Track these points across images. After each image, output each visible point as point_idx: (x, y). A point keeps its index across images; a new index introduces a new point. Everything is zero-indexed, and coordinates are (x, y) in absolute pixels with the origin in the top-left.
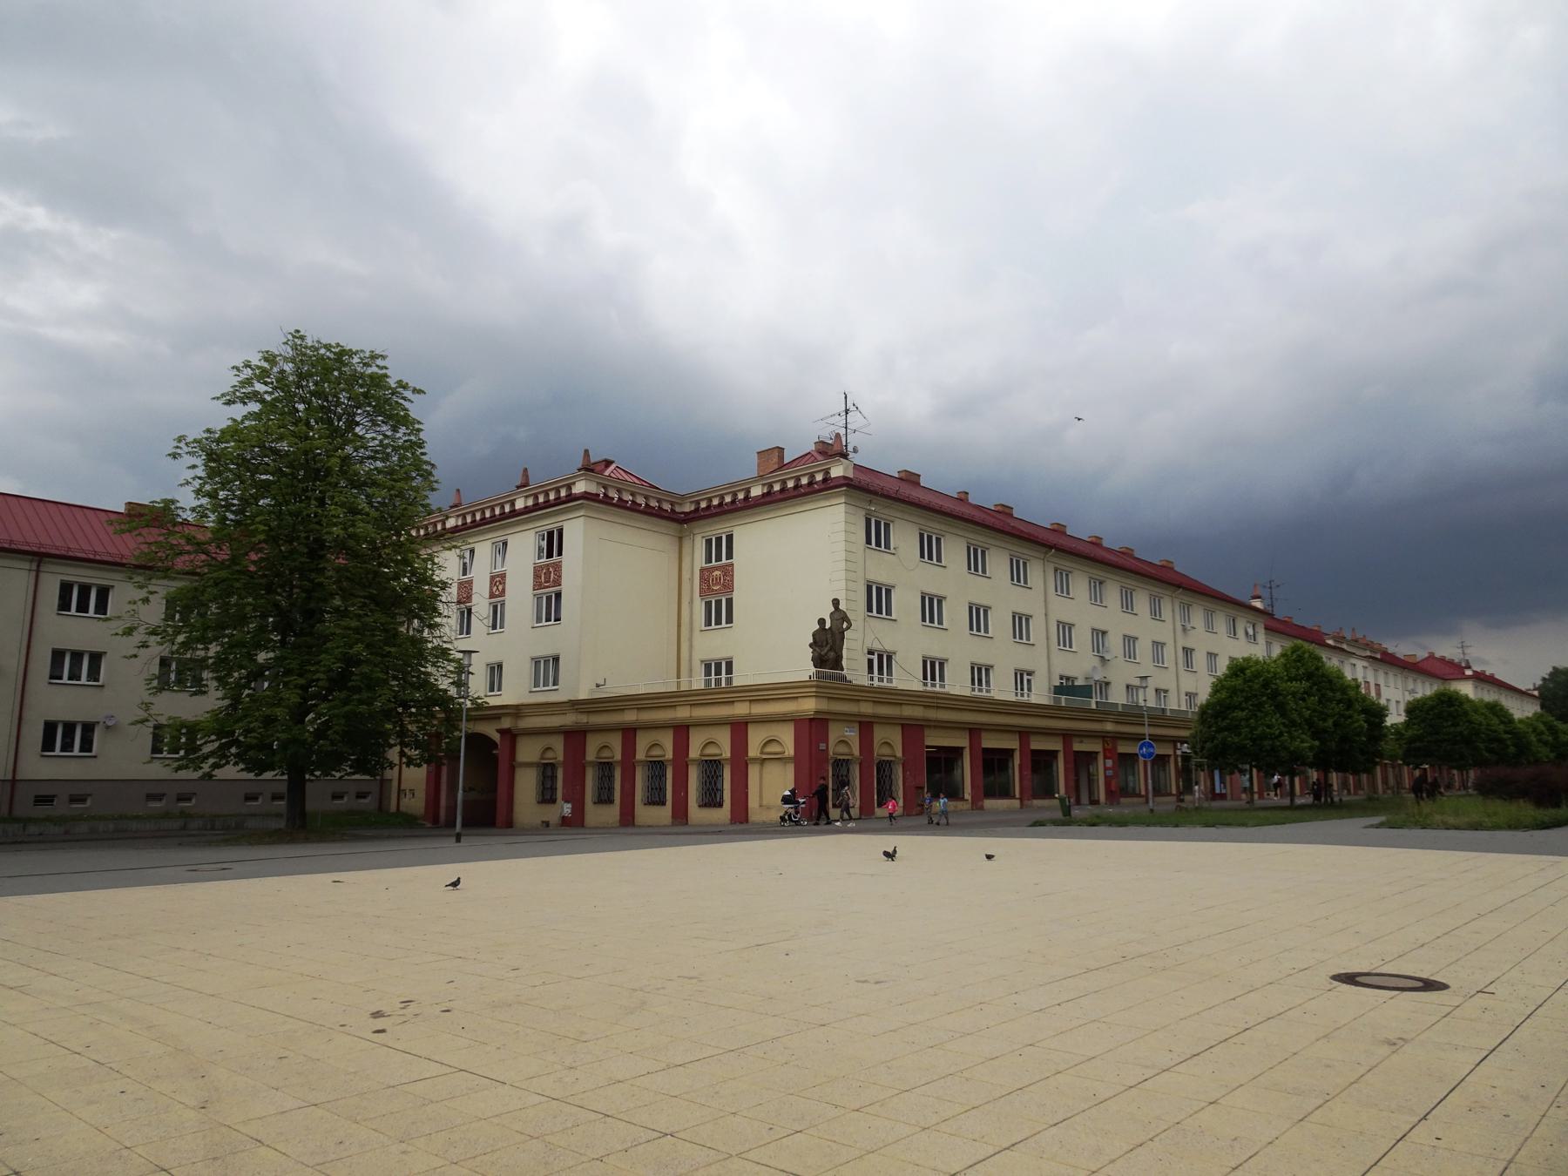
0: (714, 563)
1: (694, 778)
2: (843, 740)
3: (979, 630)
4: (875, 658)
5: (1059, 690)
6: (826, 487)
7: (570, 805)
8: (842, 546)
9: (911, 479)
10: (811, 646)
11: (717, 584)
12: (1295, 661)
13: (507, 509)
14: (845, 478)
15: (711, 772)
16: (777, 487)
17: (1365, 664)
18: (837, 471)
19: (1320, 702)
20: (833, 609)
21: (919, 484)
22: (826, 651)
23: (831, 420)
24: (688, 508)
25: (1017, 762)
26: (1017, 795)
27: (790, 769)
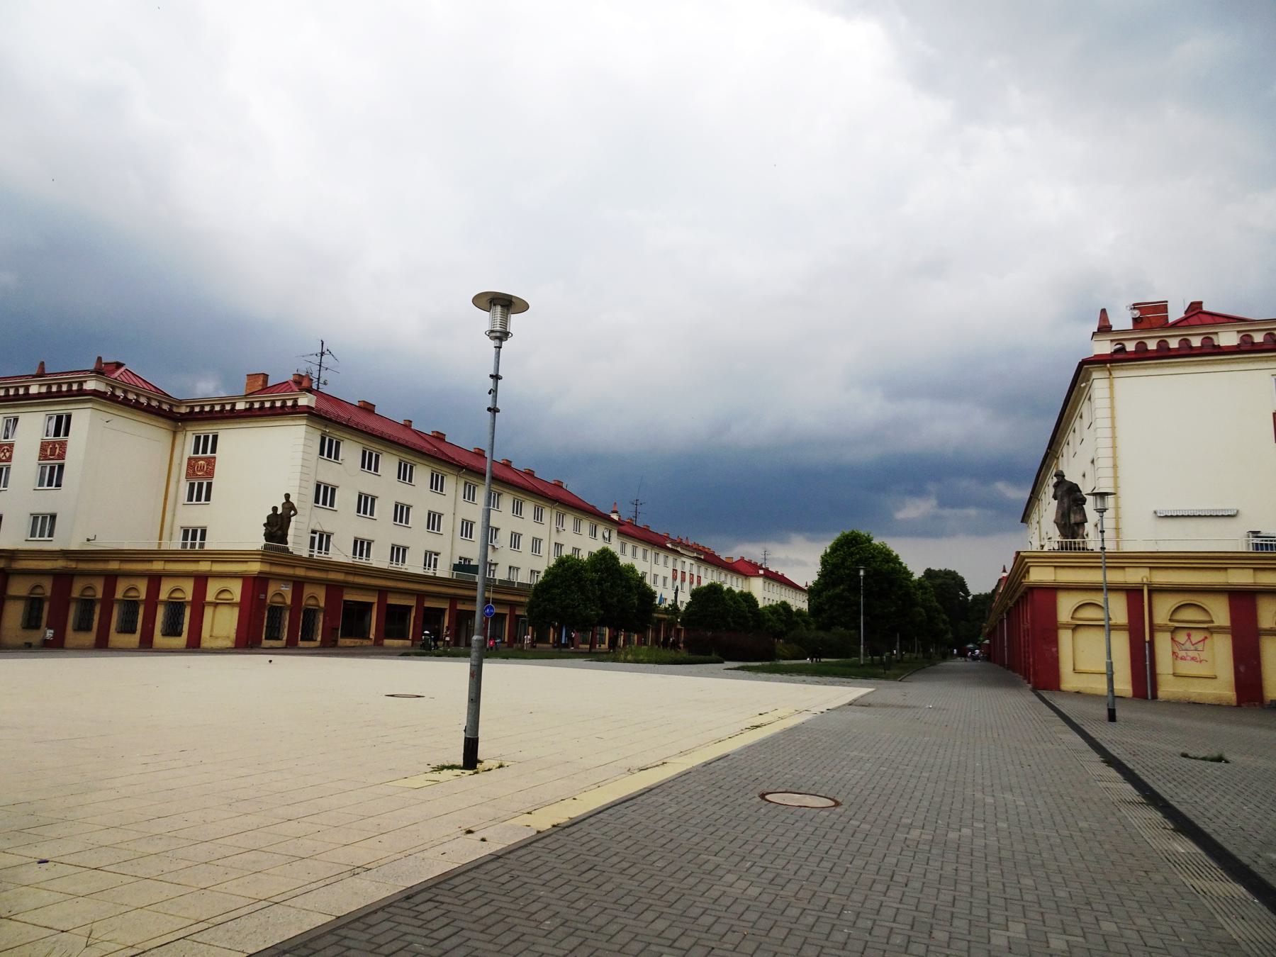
0: (200, 454)
1: (161, 613)
2: (280, 593)
3: (401, 521)
4: (317, 536)
5: (456, 567)
6: (294, 411)
7: (52, 631)
8: (300, 455)
9: (368, 408)
10: (265, 525)
11: (201, 470)
12: (601, 559)
13: (21, 391)
14: (308, 407)
15: (175, 610)
16: (257, 406)
17: (693, 562)
18: (305, 400)
19: (611, 586)
20: (285, 501)
21: (373, 412)
22: (275, 529)
23: (310, 359)
24: (184, 410)
25: (413, 615)
26: (410, 638)
27: (236, 611)
